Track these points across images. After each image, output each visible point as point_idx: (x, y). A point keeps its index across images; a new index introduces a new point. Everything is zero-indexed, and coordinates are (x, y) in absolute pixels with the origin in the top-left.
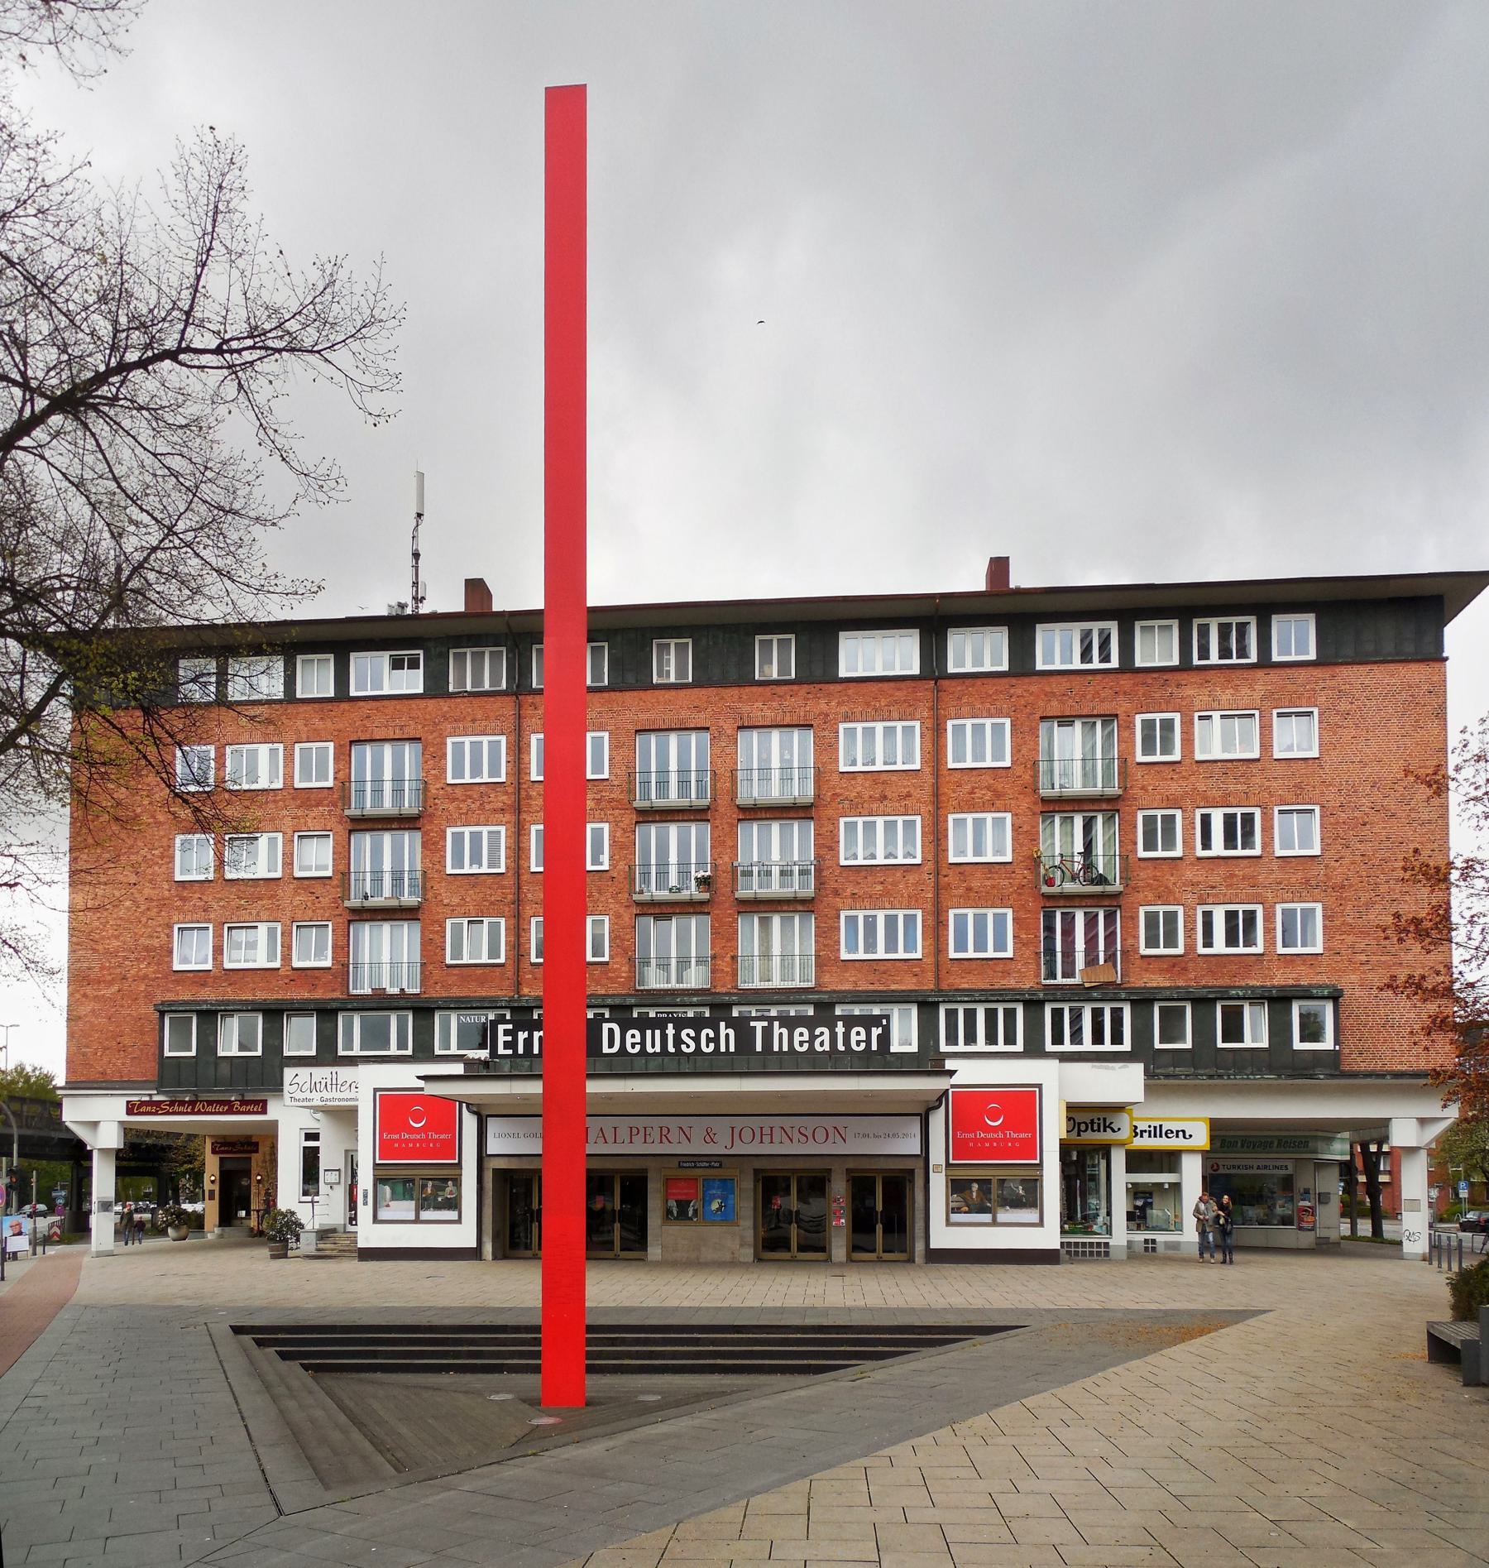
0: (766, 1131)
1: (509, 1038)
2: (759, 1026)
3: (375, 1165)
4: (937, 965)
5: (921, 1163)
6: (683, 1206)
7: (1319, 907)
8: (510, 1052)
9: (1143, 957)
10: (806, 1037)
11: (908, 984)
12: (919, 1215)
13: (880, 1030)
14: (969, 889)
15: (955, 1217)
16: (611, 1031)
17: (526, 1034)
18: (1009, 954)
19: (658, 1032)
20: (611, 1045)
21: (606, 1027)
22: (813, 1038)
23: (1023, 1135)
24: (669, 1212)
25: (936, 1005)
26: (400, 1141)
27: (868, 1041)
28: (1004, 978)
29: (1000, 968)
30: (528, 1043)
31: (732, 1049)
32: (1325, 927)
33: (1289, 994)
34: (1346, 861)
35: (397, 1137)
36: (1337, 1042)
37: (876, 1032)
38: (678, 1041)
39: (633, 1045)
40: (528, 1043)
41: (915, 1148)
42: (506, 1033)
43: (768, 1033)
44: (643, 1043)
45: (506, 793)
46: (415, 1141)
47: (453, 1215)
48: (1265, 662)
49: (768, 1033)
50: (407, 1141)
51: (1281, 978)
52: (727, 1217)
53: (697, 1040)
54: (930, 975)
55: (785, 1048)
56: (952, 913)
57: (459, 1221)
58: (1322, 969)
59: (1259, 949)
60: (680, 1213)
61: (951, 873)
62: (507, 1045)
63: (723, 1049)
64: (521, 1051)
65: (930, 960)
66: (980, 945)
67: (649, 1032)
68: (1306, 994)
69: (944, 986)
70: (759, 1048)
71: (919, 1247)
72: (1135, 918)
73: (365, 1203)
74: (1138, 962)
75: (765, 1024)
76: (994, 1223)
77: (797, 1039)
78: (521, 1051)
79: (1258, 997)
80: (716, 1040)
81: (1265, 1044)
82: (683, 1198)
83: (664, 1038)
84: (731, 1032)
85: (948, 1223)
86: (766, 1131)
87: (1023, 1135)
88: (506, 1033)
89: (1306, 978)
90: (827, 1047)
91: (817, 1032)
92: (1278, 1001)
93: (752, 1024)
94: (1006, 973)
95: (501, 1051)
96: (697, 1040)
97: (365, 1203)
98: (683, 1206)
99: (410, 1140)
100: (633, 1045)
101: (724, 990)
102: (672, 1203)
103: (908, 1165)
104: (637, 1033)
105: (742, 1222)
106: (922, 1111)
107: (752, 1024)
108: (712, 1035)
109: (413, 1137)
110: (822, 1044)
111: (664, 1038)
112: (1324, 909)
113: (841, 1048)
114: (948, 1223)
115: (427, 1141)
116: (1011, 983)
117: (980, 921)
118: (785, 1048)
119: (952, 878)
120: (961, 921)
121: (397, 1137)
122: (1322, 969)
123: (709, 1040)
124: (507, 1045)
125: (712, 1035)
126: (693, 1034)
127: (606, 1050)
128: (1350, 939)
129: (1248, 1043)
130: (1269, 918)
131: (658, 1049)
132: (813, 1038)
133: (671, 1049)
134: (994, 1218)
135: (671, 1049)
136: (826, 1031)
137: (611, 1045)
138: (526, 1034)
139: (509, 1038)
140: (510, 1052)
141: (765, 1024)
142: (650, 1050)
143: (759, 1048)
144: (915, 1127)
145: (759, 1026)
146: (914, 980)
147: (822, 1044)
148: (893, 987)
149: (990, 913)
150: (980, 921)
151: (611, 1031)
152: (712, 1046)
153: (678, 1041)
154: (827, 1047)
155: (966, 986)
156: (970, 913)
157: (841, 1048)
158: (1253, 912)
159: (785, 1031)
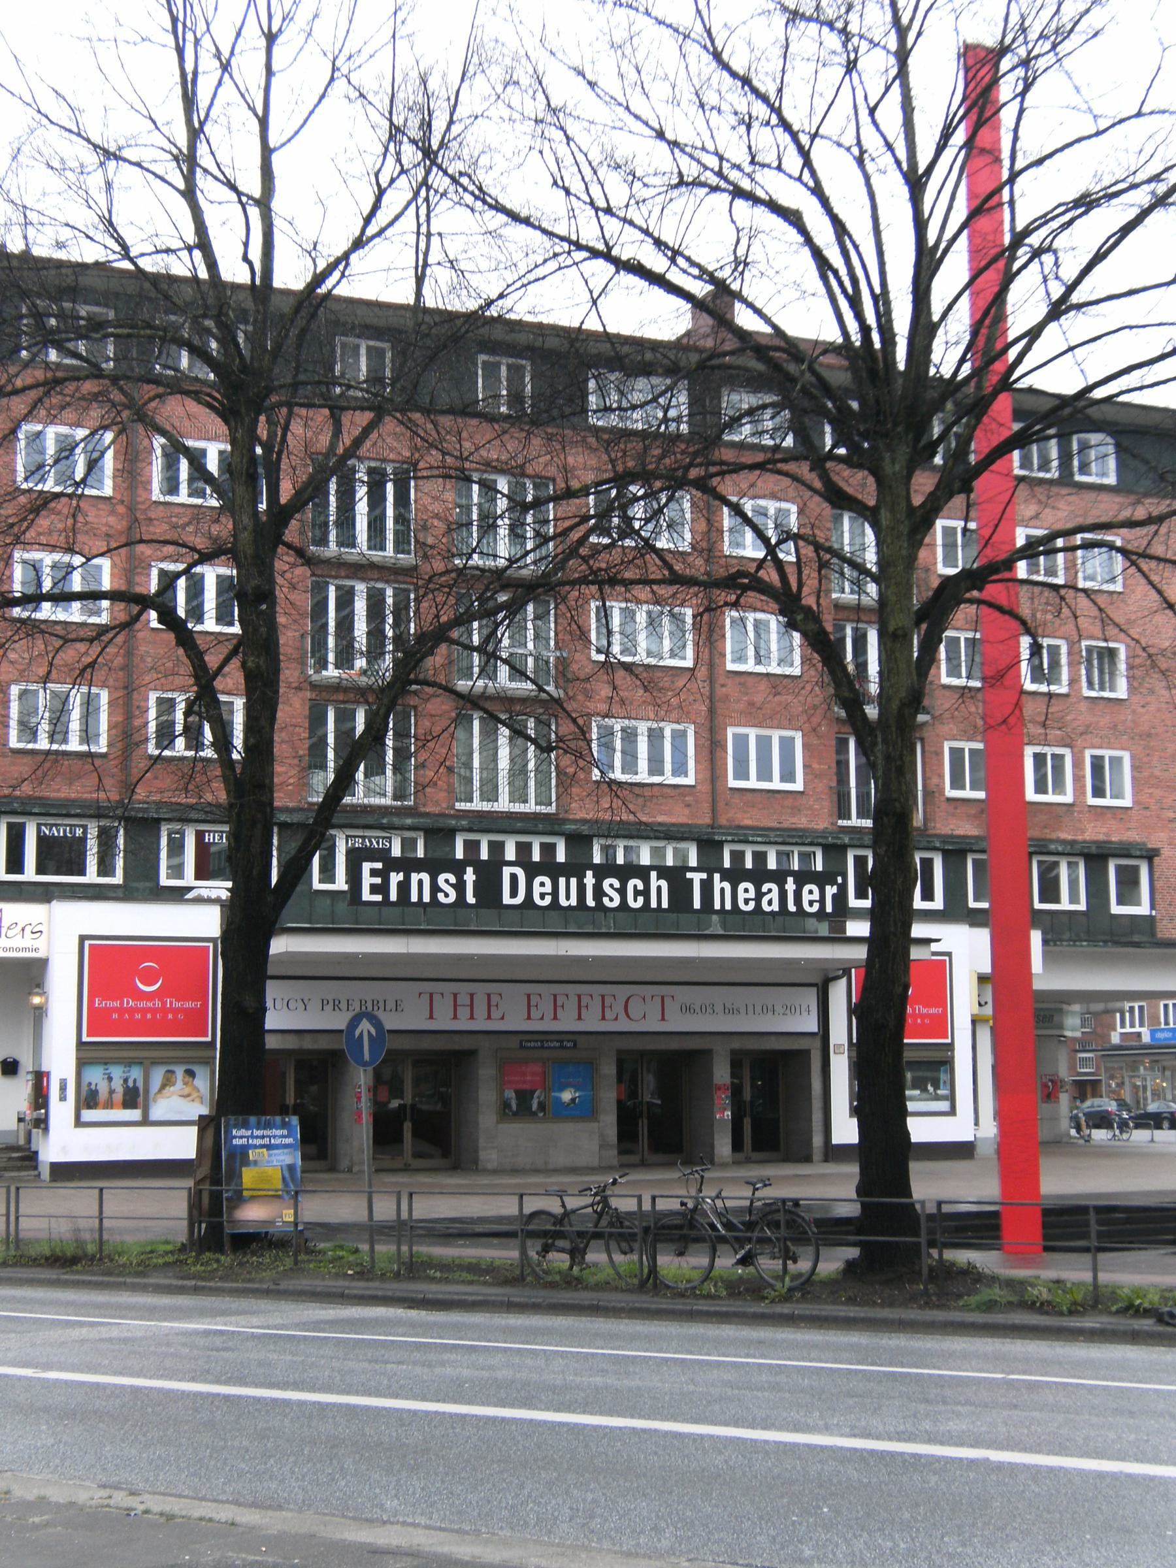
0: (464, 999)
1: (378, 880)
2: (697, 878)
3: (80, 1044)
4: (713, 792)
5: (815, 1046)
6: (524, 1097)
7: (1126, 757)
8: (378, 898)
9: (949, 800)
10: (752, 894)
11: (677, 815)
12: (817, 1104)
13: (835, 889)
14: (751, 704)
15: (88, 1115)
16: (514, 878)
17: (401, 876)
18: (798, 786)
19: (573, 881)
20: (514, 894)
21: (507, 871)
22: (759, 895)
23: (933, 1011)
24: (506, 1105)
25: (720, 845)
26: (121, 1010)
27: (822, 901)
28: (793, 815)
29: (789, 802)
30: (404, 887)
31: (665, 905)
32: (1134, 778)
33: (1106, 852)
34: (1152, 708)
35: (117, 1004)
36: (1152, 907)
37: (831, 891)
38: (599, 893)
39: (542, 896)
40: (404, 887)
41: (810, 1024)
42: (374, 873)
43: (707, 886)
44: (555, 893)
45: (112, 512)
46: (144, 1011)
47: (944, 1106)
48: (1066, 478)
49: (707, 886)
50: (132, 1011)
51: (1092, 833)
52: (586, 1111)
53: (622, 892)
54: (706, 807)
55: (728, 906)
56: (730, 731)
57: (952, 1112)
58: (1132, 825)
59: (1068, 798)
60: (522, 1108)
61: (729, 682)
62: (374, 889)
63: (654, 905)
64: (393, 896)
65: (705, 788)
66: (765, 773)
67: (562, 881)
68: (1124, 851)
69: (723, 821)
70: (697, 905)
71: (817, 1140)
72: (940, 753)
73: (63, 1098)
74: (944, 806)
75: (704, 876)
76: (145, 1122)
77: (741, 896)
78: (393, 896)
79: (1074, 851)
80: (646, 893)
81: (1082, 907)
82: (526, 1087)
83: (581, 888)
84: (664, 884)
85: (79, 1123)
86: (464, 999)
87: (933, 1011)
88: (374, 873)
89: (1118, 835)
90: (775, 907)
91: (765, 888)
92: (1096, 858)
93: (689, 875)
94: (795, 810)
95: (366, 896)
96: (622, 892)
97: (63, 1098)
98: (524, 1097)
99: (139, 1010)
100: (542, 896)
101: (436, 810)
102: (510, 1094)
103: (802, 1044)
104: (547, 880)
105: (602, 1117)
106: (817, 979)
107: (689, 875)
108: (641, 887)
109: (142, 1004)
110: (770, 903)
111: (581, 888)
112: (1133, 758)
113: (792, 908)
114: (79, 1123)
115: (164, 1010)
116: (802, 822)
117: (764, 745)
118: (728, 906)
119: (730, 688)
120: (742, 741)
121: (117, 1004)
122: (1132, 825)
123: (637, 893)
124: (374, 889)
125: (641, 887)
126: (617, 884)
127: (507, 900)
128: (1158, 793)
129: (1065, 905)
130: (1078, 764)
131: (573, 901)
132: (759, 895)
133: (591, 903)
134: (146, 1114)
135: (591, 903)
136: (774, 887)
137: (514, 894)
138: (401, 876)
139: (378, 880)
140: (378, 898)
141: (704, 876)
142: (563, 902)
143: (697, 905)
144: (810, 998)
145: (697, 878)
146: (687, 811)
147: (770, 903)
148: (660, 819)
149: (776, 735)
150: (764, 745)
151: (514, 878)
152: (641, 899)
153: (599, 893)
154: (775, 907)
155: (748, 822)
156: (752, 733)
157: (792, 908)
158: (1062, 757)
159: (727, 886)
